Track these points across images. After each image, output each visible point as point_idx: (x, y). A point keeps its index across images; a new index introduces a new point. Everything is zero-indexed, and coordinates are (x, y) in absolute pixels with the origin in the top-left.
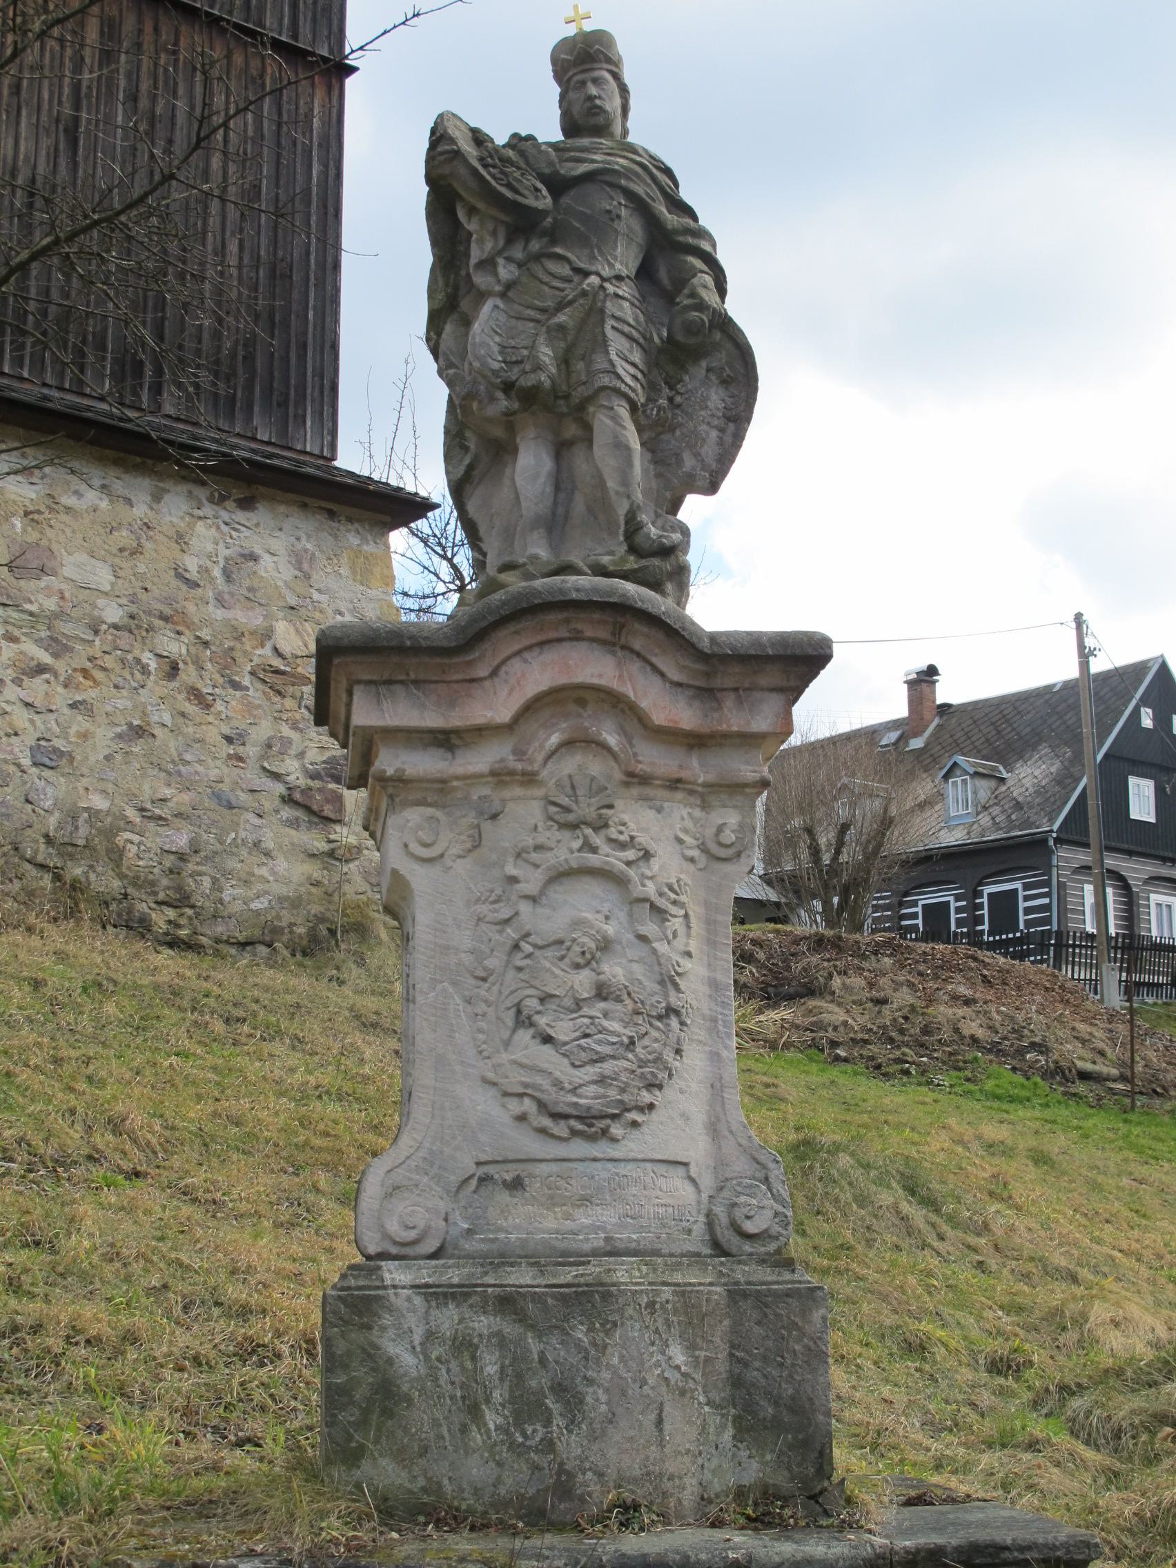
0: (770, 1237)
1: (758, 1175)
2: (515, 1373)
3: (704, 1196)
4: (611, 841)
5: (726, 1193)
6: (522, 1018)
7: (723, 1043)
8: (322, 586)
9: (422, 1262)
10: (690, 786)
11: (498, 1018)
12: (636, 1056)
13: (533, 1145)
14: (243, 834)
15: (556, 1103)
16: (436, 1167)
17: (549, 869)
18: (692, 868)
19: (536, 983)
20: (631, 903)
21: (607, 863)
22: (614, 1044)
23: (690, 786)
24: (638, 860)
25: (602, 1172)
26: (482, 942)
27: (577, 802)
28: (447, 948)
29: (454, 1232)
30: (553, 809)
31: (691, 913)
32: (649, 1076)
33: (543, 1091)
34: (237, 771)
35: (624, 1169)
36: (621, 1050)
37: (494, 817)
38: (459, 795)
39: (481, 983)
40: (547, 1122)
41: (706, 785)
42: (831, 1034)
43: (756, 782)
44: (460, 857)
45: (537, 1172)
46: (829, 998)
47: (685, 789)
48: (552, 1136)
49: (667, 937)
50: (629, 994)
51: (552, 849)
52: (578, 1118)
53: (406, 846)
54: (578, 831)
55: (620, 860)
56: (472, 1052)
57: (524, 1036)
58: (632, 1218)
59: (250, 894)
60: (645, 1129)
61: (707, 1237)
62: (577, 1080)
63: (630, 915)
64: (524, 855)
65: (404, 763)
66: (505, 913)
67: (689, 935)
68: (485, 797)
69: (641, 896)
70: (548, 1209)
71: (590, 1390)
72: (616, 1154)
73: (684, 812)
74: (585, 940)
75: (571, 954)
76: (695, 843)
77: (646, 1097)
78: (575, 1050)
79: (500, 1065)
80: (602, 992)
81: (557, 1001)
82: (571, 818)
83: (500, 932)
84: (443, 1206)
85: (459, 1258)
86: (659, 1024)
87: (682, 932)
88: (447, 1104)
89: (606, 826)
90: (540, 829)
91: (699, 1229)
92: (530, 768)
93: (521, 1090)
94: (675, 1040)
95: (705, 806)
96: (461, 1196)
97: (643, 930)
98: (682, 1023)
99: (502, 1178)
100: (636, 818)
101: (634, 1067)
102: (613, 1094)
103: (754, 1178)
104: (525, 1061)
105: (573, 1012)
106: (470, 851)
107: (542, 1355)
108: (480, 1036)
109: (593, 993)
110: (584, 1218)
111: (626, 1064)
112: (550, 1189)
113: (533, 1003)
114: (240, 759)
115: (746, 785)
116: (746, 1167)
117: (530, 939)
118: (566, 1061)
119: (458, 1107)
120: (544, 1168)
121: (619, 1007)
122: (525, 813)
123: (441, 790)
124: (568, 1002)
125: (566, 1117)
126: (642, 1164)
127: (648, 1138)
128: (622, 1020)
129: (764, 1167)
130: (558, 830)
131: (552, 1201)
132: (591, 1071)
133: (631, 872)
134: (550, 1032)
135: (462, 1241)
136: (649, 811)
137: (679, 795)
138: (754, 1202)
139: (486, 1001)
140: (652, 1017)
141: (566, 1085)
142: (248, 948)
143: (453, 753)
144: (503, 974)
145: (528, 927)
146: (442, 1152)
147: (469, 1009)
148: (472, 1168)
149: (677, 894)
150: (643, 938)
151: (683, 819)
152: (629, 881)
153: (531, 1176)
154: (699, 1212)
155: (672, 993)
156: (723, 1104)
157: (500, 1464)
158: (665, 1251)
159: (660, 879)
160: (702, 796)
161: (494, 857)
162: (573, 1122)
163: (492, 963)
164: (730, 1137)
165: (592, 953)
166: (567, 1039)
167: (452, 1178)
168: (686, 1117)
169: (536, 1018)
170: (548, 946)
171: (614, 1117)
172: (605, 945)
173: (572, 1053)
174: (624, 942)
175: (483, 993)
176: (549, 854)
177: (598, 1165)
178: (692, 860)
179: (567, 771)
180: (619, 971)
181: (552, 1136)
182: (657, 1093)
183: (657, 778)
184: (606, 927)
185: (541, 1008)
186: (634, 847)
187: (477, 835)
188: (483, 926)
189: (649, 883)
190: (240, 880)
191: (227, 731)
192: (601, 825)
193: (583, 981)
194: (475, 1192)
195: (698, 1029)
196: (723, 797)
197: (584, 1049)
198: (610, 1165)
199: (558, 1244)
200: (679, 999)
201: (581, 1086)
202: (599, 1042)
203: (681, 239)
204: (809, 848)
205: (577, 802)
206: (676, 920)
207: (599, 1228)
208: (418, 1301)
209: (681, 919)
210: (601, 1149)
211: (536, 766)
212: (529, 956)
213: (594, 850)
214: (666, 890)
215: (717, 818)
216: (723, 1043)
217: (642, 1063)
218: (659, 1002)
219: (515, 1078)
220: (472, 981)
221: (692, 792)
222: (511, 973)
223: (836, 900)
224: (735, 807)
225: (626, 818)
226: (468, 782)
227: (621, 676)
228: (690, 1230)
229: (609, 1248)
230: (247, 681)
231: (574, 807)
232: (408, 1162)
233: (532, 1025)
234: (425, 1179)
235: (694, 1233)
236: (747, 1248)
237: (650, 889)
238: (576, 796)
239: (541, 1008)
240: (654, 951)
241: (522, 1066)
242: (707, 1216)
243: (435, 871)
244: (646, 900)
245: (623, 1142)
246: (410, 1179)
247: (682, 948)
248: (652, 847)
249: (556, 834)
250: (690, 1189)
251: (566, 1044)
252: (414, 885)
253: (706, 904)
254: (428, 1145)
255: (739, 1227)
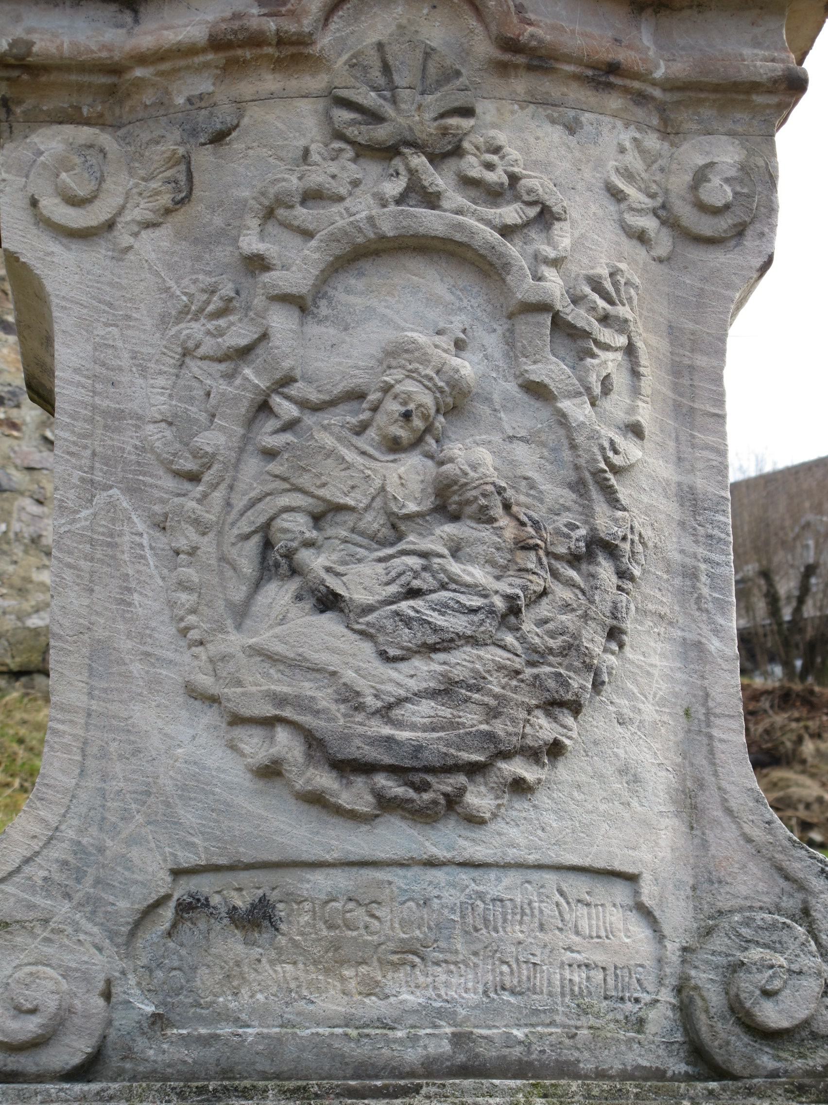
0: (815, 1036)
1: (788, 903)
3: (672, 948)
4: (468, 183)
5: (719, 942)
6: (275, 555)
7: (711, 622)
9: (52, 1088)
10: (636, 85)
11: (222, 559)
12: (522, 639)
13: (296, 832)
14: (16, 526)
15: (346, 738)
16: (89, 880)
17: (333, 238)
18: (641, 253)
19: (305, 480)
20: (511, 316)
21: (460, 227)
22: (474, 611)
23: (636, 85)
24: (527, 224)
25: (448, 889)
26: (191, 400)
27: (394, 101)
28: (120, 415)
29: (124, 1021)
30: (344, 115)
31: (640, 344)
32: (551, 684)
33: (317, 713)
34: (9, 442)
35: (496, 885)
36: (490, 626)
37: (219, 138)
38: (148, 97)
39: (187, 486)
40: (324, 780)
41: (671, 85)
42: (802, 813)
43: (775, 81)
44: (149, 225)
45: (305, 889)
46: (798, 767)
47: (626, 90)
48: (339, 811)
49: (588, 389)
50: (507, 507)
51: (341, 199)
52: (393, 770)
53: (34, 203)
54: (397, 162)
55: (488, 223)
56: (166, 632)
57: (278, 595)
58: (513, 992)
59: (26, 606)
60: (541, 798)
61: (679, 1037)
62: (390, 688)
63: (510, 341)
64: (281, 212)
65: (30, 31)
66: (239, 334)
67: (636, 392)
68: (201, 97)
69: (533, 299)
70: (327, 971)
72: (480, 853)
73: (626, 137)
74: (410, 386)
75: (381, 419)
76: (649, 203)
77: (545, 728)
78: (389, 624)
79: (224, 658)
80: (450, 501)
81: (350, 519)
82: (381, 133)
83: (229, 377)
84: (101, 963)
85: (134, 1078)
86: (572, 573)
87: (621, 380)
88: (113, 747)
89: (457, 152)
90: (315, 157)
91: (660, 1018)
92: (293, 28)
93: (269, 710)
94: (607, 608)
95: (669, 131)
96: (139, 943)
97: (538, 372)
98: (623, 574)
99: (224, 903)
100: (520, 137)
101: (518, 663)
102: (472, 719)
103: (779, 910)
104: (279, 648)
105: (383, 543)
106: (168, 212)
108: (184, 597)
109: (428, 504)
110: (406, 993)
111: (500, 656)
112: (331, 927)
113: (298, 524)
114: (14, 426)
115: (754, 87)
116: (761, 887)
117: (293, 390)
118: (367, 647)
119: (136, 752)
120: (320, 882)
121: (485, 533)
122: (284, 129)
123: (112, 91)
124: (373, 522)
125: (367, 768)
126: (535, 875)
127: (549, 818)
128: (492, 563)
129: (801, 886)
130: (355, 160)
131: (336, 956)
132: (423, 671)
133: (513, 250)
134: (333, 583)
135: (141, 1043)
136: (548, 128)
137: (615, 102)
138: (781, 960)
139: (196, 522)
140: (557, 557)
141: (370, 701)
142: (24, 679)
143: (135, 12)
144: (236, 466)
145: (286, 364)
146: (101, 850)
147: (163, 541)
148: (162, 883)
149: (611, 303)
150: (537, 391)
151: (622, 150)
152: (507, 266)
153: (291, 898)
154: (661, 982)
155: (601, 508)
156: (711, 752)
158: (587, 1066)
159: (574, 268)
160: (662, 109)
161: (218, 221)
162: (382, 780)
163: (211, 440)
164: (726, 820)
165: (425, 417)
166: (370, 599)
167: (123, 904)
168: (630, 775)
169: (304, 555)
170: (332, 403)
171: (473, 770)
172: (456, 402)
173: (381, 629)
174: (496, 397)
175: (193, 504)
176: (336, 208)
177: (439, 875)
178: (641, 237)
179: (373, 38)
180: (486, 457)
181: (339, 811)
182: (569, 721)
183: (569, 59)
184: (456, 362)
185: (312, 535)
186: (517, 198)
187: (182, 178)
188: (194, 367)
189: (549, 273)
190: (11, 587)
192: (446, 152)
193: (407, 478)
194: (169, 934)
195: (655, 592)
196: (707, 112)
197: (407, 622)
198: (464, 876)
199: (348, 1048)
200: (616, 520)
201: (401, 701)
202: (442, 608)
204: (766, 595)
205: (394, 101)
206: (610, 355)
207: (440, 1013)
209: (619, 356)
210: (446, 840)
211: (307, 24)
212: (290, 426)
213: (432, 200)
214: (587, 290)
215: (692, 154)
216: (711, 622)
217: (537, 656)
218: (573, 527)
219: (257, 688)
220: (169, 483)
221: (641, 99)
222: (252, 465)
223: (799, 663)
224: (731, 134)
225: (501, 138)
226: (165, 66)
228: (641, 1022)
229: (461, 1058)
231: (389, 110)
232: (27, 870)
233: (294, 571)
234: (64, 908)
235: (651, 1028)
236: (767, 1061)
237: (554, 285)
238: (394, 88)
239: (315, 534)
240: (562, 419)
241: (271, 658)
242: (679, 990)
243: (94, 258)
244: (543, 307)
245: (492, 826)
246: (31, 907)
247: (621, 416)
248: (556, 200)
249: (347, 168)
250: (638, 933)
251: (368, 609)
252: (50, 286)
253: (673, 332)
254: (71, 834)
255: (749, 1014)
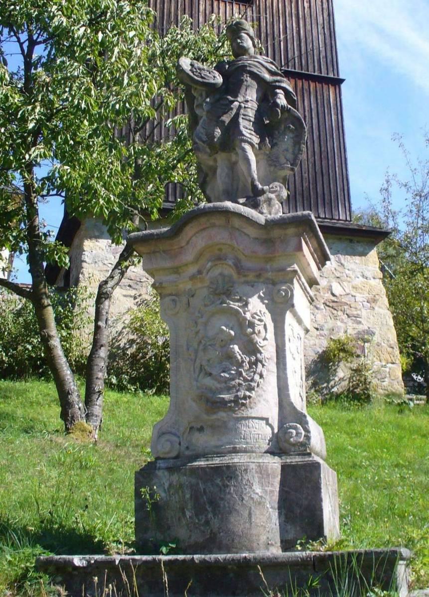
2: (196, 497)
8: (349, 268)
37: (193, 296)
71: (222, 502)
107: (204, 489)
157: (191, 531)
191: (316, 326)
203: (274, 84)
208: (166, 473)
227: (231, 238)
230: (322, 306)
